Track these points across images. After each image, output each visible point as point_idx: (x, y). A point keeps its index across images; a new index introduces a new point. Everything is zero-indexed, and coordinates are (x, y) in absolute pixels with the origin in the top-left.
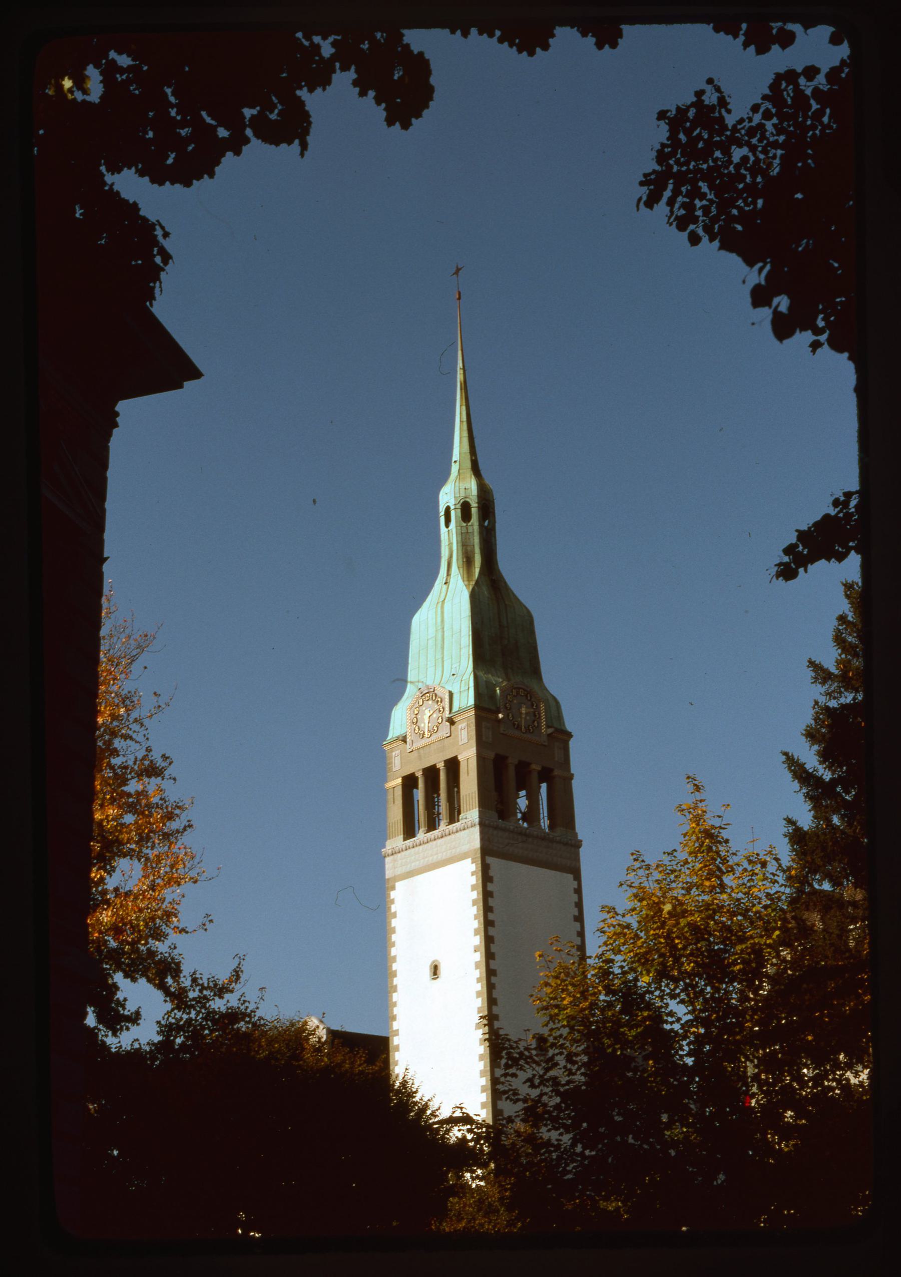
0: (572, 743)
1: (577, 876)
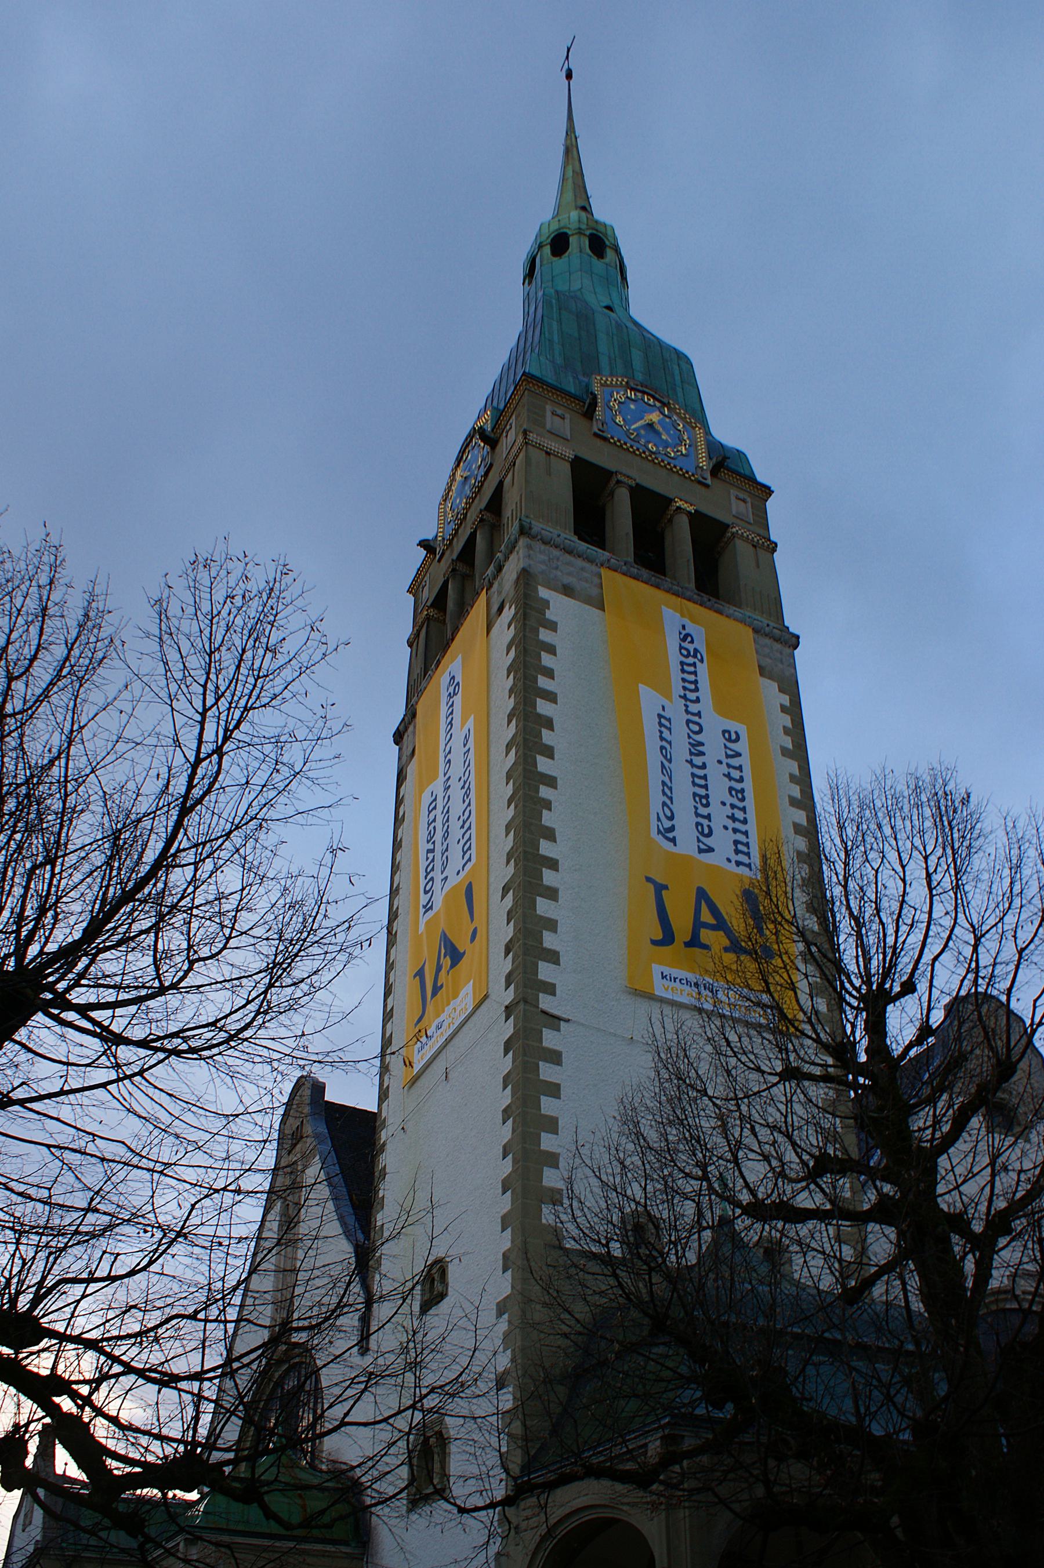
0: (771, 504)
1: (790, 687)
